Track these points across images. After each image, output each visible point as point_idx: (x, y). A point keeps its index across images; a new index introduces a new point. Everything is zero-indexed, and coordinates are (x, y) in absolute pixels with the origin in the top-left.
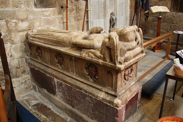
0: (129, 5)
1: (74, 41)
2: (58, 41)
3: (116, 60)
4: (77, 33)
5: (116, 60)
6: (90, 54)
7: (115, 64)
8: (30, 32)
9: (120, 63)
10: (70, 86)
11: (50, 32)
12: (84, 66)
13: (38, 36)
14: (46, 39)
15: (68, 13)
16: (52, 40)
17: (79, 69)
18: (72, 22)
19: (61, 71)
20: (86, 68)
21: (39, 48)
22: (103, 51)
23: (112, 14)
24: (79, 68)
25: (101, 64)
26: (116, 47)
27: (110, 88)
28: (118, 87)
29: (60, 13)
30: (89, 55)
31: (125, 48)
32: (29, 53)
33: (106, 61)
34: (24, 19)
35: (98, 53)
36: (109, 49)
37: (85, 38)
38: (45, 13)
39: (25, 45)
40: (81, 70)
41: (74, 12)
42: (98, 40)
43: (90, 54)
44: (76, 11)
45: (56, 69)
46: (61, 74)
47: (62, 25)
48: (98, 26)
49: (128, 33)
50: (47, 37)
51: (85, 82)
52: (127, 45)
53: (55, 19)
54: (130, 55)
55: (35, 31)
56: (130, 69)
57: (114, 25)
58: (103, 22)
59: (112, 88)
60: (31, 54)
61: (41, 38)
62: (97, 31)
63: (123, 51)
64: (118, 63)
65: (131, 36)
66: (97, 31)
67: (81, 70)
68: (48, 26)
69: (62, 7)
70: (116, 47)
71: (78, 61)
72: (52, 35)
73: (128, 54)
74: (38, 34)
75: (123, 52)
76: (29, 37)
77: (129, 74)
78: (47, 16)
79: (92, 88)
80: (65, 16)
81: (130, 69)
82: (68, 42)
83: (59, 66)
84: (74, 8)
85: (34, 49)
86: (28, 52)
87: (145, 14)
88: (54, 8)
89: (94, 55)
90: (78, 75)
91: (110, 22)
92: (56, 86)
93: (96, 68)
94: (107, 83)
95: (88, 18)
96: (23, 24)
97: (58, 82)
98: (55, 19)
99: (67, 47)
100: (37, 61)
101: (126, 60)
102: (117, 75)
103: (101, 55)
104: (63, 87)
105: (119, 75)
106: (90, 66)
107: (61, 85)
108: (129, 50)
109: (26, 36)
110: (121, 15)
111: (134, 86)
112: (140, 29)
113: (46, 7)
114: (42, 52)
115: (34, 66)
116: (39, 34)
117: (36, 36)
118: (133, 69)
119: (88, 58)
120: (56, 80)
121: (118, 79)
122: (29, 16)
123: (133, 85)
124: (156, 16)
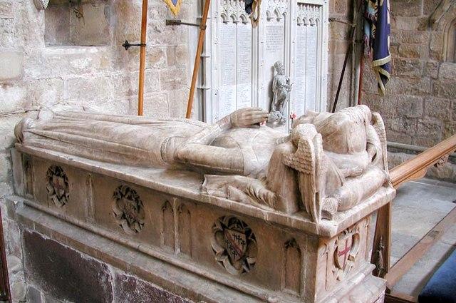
0: (327, 41)
1: (182, 150)
2: (126, 150)
3: (315, 207)
4: (186, 126)
5: (315, 207)
6: (234, 189)
7: (311, 217)
8: (30, 121)
9: (327, 215)
10: (161, 289)
11: (97, 122)
12: (209, 224)
13: (58, 133)
14: (85, 142)
15: (146, 64)
16: (103, 146)
17: (194, 237)
18: (156, 92)
19: (131, 243)
20: (217, 233)
21: (57, 169)
22: (275, 180)
23: (276, 68)
24: (194, 231)
25: (266, 218)
26: (314, 169)
27: (294, 293)
28: (318, 289)
29: (120, 63)
30: (227, 192)
31: (341, 173)
32: (22, 184)
33: (283, 210)
34: (11, 79)
35: (259, 188)
36: (295, 175)
37: (215, 142)
38: (75, 63)
39: (10, 159)
40: (201, 239)
41: (163, 59)
42: (256, 149)
43: (234, 189)
44: (168, 58)
45: (115, 236)
46: (131, 254)
47: (124, 100)
48: (233, 109)
49: (347, 127)
50: (88, 136)
51: (212, 277)
52: (344, 162)
53: (105, 82)
54: (354, 192)
55: (46, 117)
56: (349, 236)
57: (281, 101)
58: (248, 94)
59: (299, 292)
60: (28, 190)
61: (66, 139)
62: (251, 119)
63: (333, 179)
64: (320, 217)
65: (356, 137)
66: (251, 119)
67: (201, 239)
68: (86, 103)
69: (127, 46)
70: (314, 169)
71: (189, 212)
72: (106, 131)
73: (350, 189)
74: (56, 128)
75: (335, 184)
76: (26, 135)
77: (347, 250)
78: (82, 72)
79: (235, 295)
80: (135, 73)
81: (349, 236)
82: (157, 152)
83: (126, 227)
84: (164, 47)
85: (41, 175)
86: (19, 182)
87: (375, 69)
88: (104, 49)
89: (246, 193)
90: (187, 256)
91: (271, 94)
92: (111, 291)
93: (248, 233)
94: (283, 277)
95: (203, 82)
96: (9, 94)
97: (118, 279)
98: (105, 82)
99: (155, 168)
100: (50, 210)
101: (342, 208)
102: (316, 252)
103: (267, 191)
104: (136, 295)
105: (321, 250)
106: (229, 225)
107: (130, 286)
108: (351, 177)
109: (18, 130)
110: (303, 71)
111: (362, 287)
112: (377, 115)
113: (74, 43)
114: (66, 184)
115: (39, 226)
116: (61, 127)
117: (49, 132)
118: (358, 234)
119: (227, 200)
120: (112, 271)
121: (319, 265)
122: (27, 71)
123: (360, 284)
124: (408, 76)
